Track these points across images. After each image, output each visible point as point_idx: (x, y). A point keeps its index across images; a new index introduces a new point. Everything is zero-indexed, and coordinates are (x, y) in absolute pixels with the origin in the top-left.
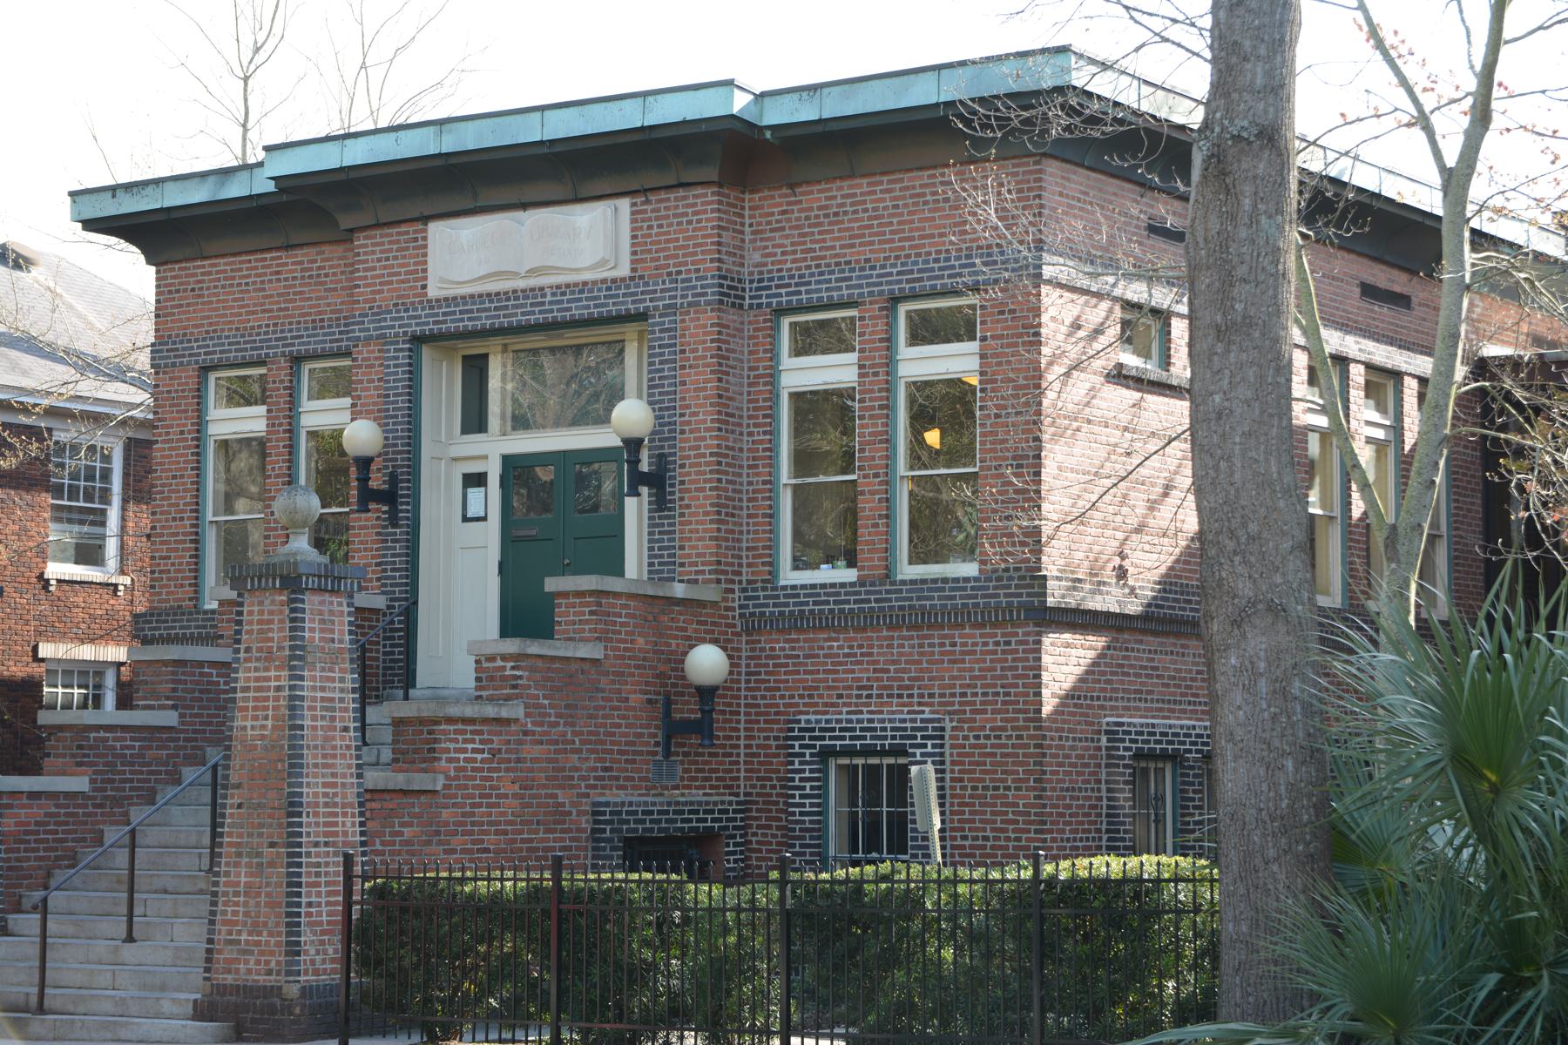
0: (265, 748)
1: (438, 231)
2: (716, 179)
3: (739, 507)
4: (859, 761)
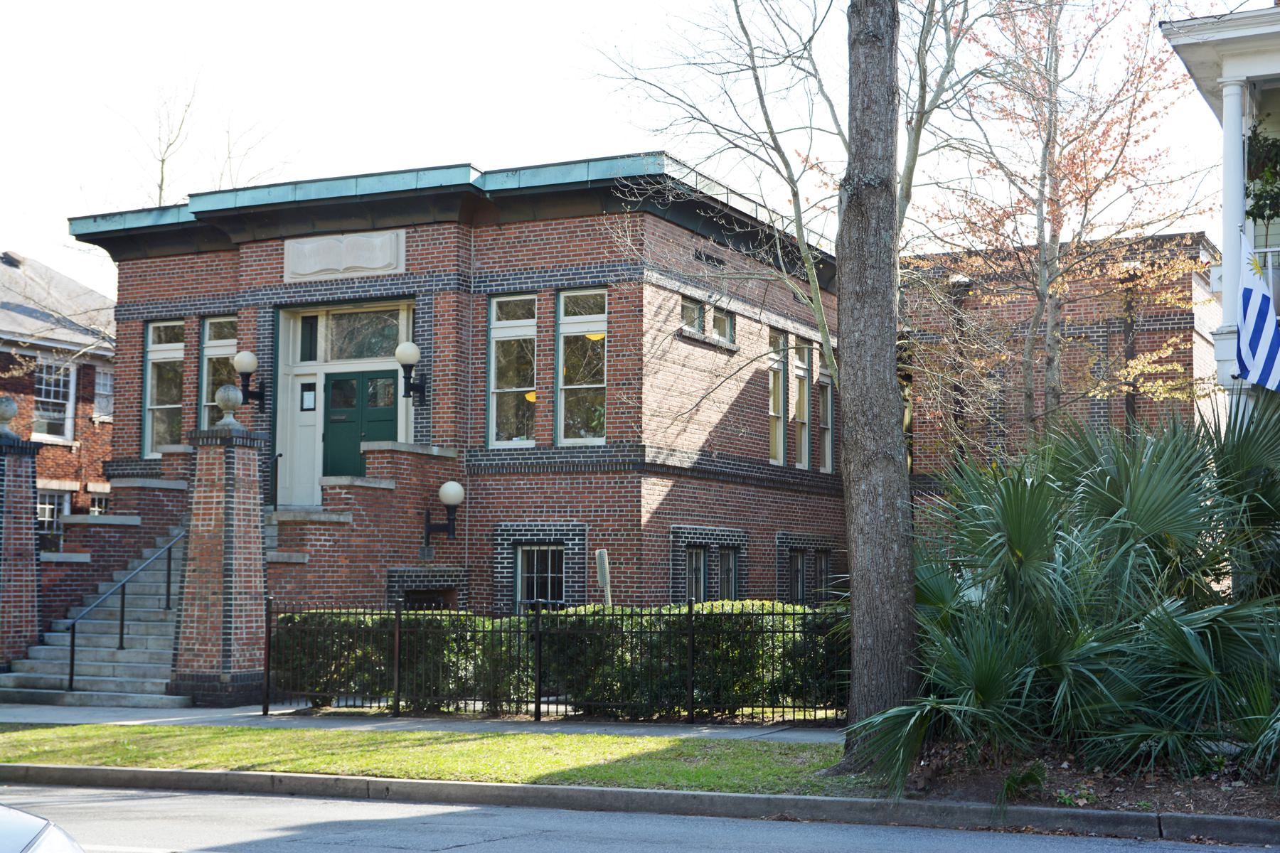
0: (210, 537)
1: (290, 245)
2: (456, 219)
3: (468, 403)
4: (535, 548)
